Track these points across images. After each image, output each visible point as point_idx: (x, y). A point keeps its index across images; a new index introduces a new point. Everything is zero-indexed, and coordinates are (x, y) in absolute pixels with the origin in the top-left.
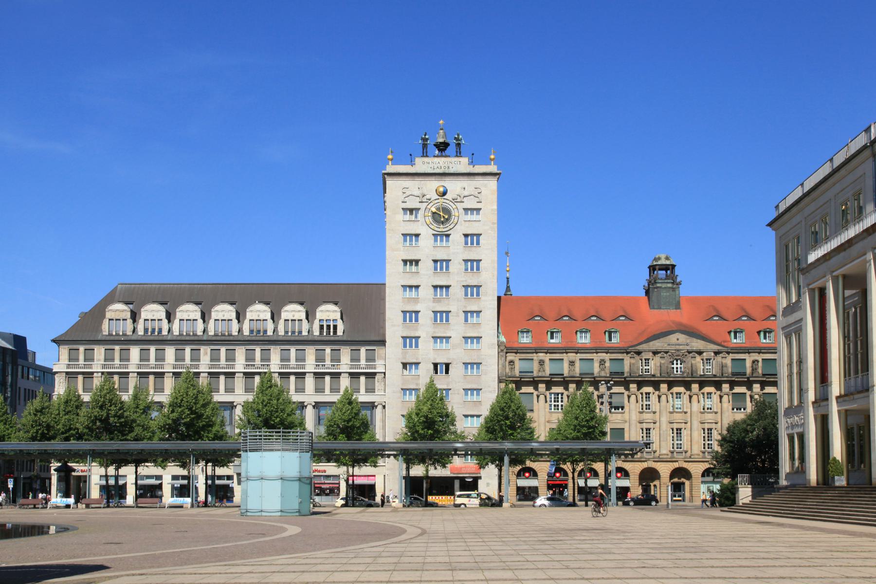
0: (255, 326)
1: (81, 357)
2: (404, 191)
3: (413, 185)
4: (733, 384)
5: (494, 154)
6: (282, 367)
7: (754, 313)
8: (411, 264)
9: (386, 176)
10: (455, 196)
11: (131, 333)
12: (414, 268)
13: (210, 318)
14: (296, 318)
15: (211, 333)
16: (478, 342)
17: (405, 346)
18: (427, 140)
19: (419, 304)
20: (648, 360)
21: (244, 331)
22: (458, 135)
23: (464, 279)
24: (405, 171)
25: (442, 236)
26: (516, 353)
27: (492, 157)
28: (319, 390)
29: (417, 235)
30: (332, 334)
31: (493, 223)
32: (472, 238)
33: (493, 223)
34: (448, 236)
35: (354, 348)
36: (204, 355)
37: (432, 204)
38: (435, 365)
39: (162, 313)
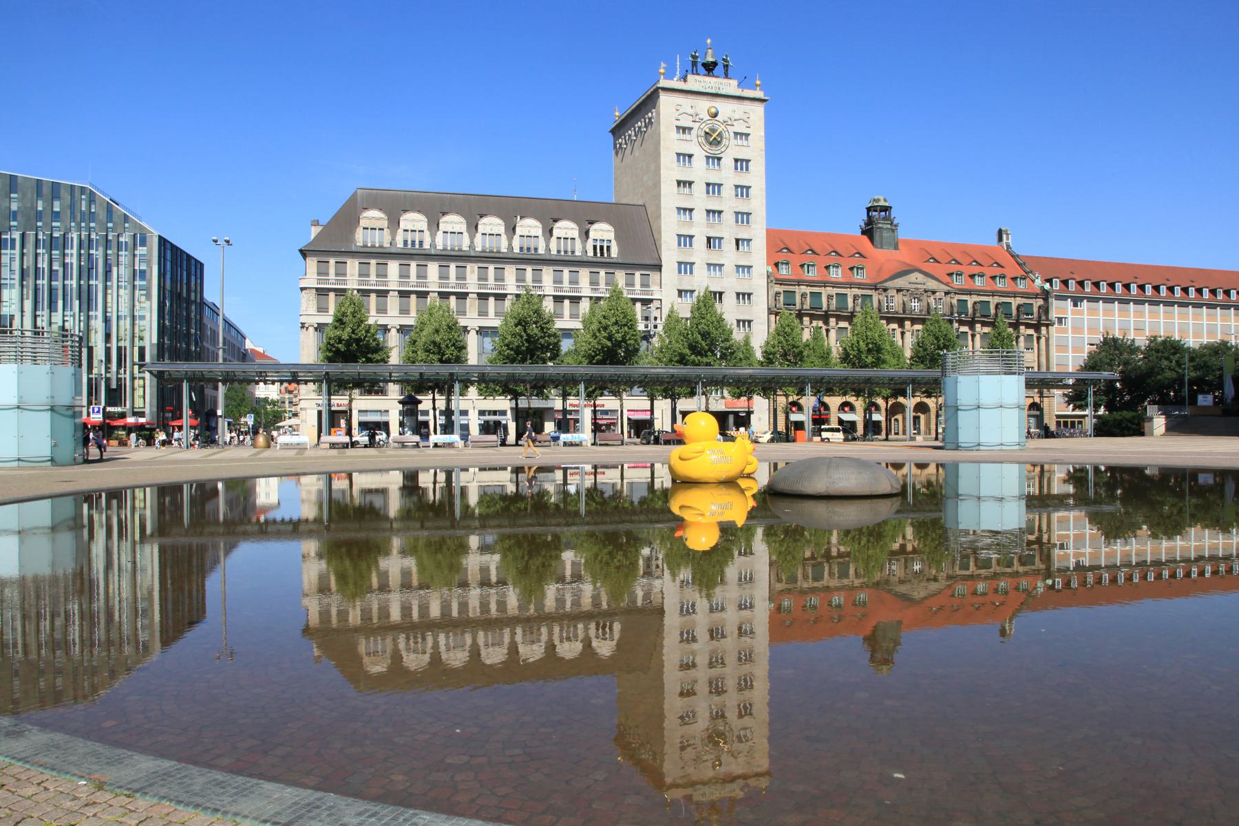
0: (526, 243)
1: (332, 271)
2: (677, 108)
3: (686, 102)
5: (759, 79)
8: (684, 186)
10: (726, 119)
12: (687, 190)
14: (569, 236)
16: (720, 270)
18: (697, 57)
23: (734, 205)
25: (713, 158)
27: (758, 82)
28: (404, 311)
29: (690, 156)
30: (599, 255)
32: (741, 164)
33: (761, 150)
34: (719, 159)
35: (339, 260)
37: (704, 124)
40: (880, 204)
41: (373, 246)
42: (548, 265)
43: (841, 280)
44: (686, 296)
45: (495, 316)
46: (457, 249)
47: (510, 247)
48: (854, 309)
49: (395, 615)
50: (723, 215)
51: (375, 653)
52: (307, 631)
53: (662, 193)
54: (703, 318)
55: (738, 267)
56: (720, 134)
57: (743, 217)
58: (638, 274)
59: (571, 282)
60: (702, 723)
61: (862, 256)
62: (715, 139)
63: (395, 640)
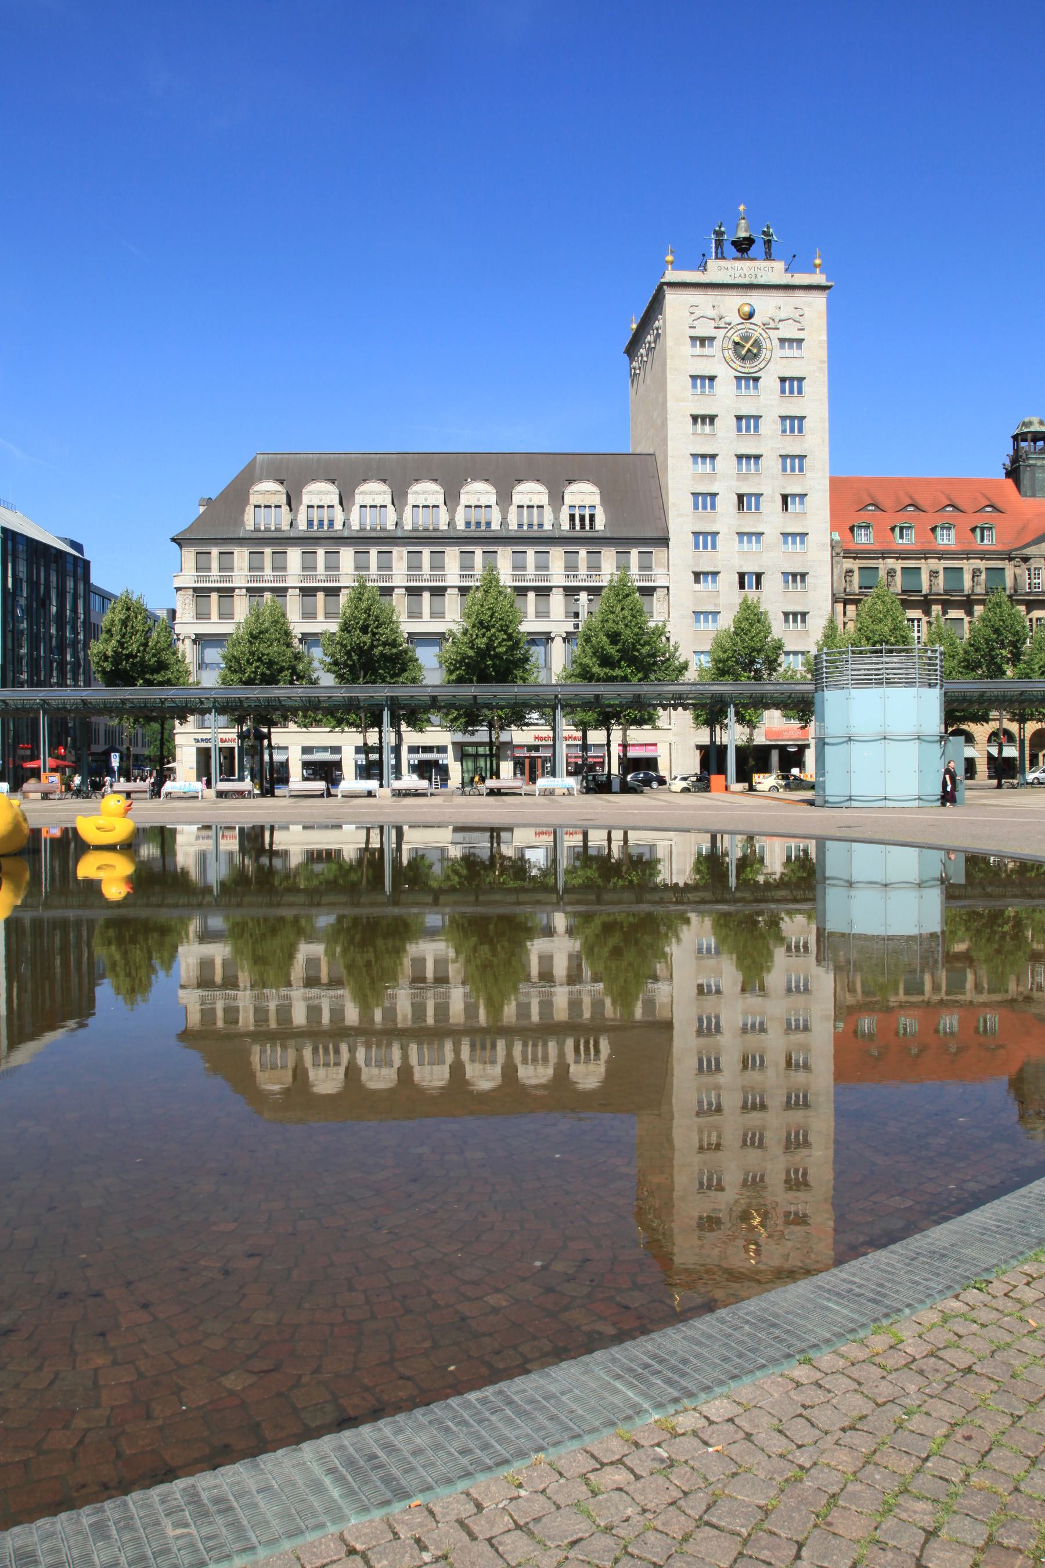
0: (474, 516)
1: (215, 564)
2: (692, 310)
3: (704, 300)
4: (947, 605)
5: (820, 257)
6: (305, 578)
7: (887, 502)
8: (703, 423)
9: (665, 287)
10: (766, 320)
11: (288, 528)
12: (707, 428)
13: (300, 502)
14: (535, 503)
15: (356, 526)
16: (802, 542)
17: (697, 546)
18: (723, 233)
19: (717, 483)
20: (1039, 569)
21: (458, 523)
22: (768, 228)
24: (694, 281)
25: (747, 379)
26: (855, 558)
27: (818, 261)
29: (712, 379)
31: (822, 362)
32: (791, 384)
33: (822, 362)
34: (756, 380)
35: (592, 549)
36: (398, 560)
37: (733, 331)
38: (742, 576)
39: (333, 496)
40: (1032, 429)
41: (267, 530)
42: (505, 544)
43: (954, 548)
44: (706, 581)
45: (431, 617)
46: (431, 528)
47: (451, 523)
48: (973, 590)
49: (299, 1017)
50: (762, 461)
51: (274, 1067)
52: (186, 1036)
53: (669, 435)
54: (613, 613)
55: (785, 535)
56: (757, 343)
57: (793, 462)
58: (634, 552)
59: (537, 568)
60: (731, 1195)
61: (996, 509)
62: (749, 350)
63: (299, 1050)
